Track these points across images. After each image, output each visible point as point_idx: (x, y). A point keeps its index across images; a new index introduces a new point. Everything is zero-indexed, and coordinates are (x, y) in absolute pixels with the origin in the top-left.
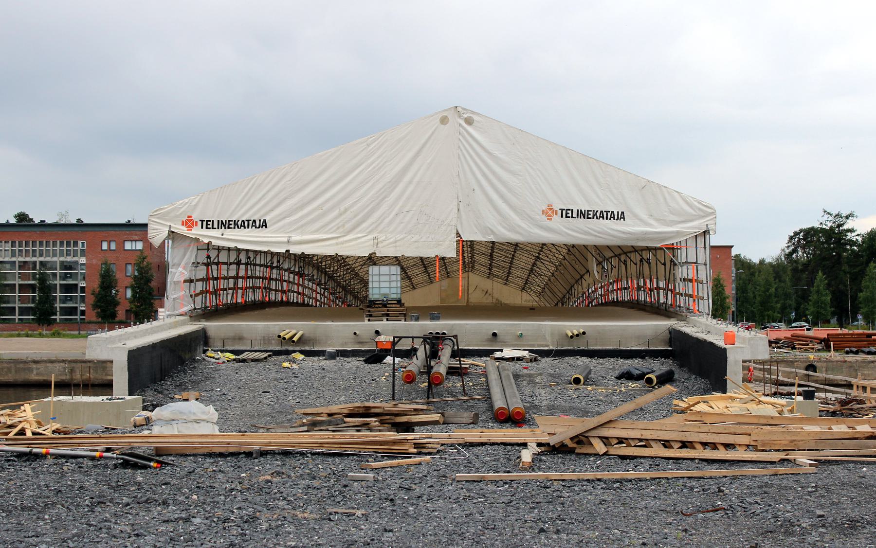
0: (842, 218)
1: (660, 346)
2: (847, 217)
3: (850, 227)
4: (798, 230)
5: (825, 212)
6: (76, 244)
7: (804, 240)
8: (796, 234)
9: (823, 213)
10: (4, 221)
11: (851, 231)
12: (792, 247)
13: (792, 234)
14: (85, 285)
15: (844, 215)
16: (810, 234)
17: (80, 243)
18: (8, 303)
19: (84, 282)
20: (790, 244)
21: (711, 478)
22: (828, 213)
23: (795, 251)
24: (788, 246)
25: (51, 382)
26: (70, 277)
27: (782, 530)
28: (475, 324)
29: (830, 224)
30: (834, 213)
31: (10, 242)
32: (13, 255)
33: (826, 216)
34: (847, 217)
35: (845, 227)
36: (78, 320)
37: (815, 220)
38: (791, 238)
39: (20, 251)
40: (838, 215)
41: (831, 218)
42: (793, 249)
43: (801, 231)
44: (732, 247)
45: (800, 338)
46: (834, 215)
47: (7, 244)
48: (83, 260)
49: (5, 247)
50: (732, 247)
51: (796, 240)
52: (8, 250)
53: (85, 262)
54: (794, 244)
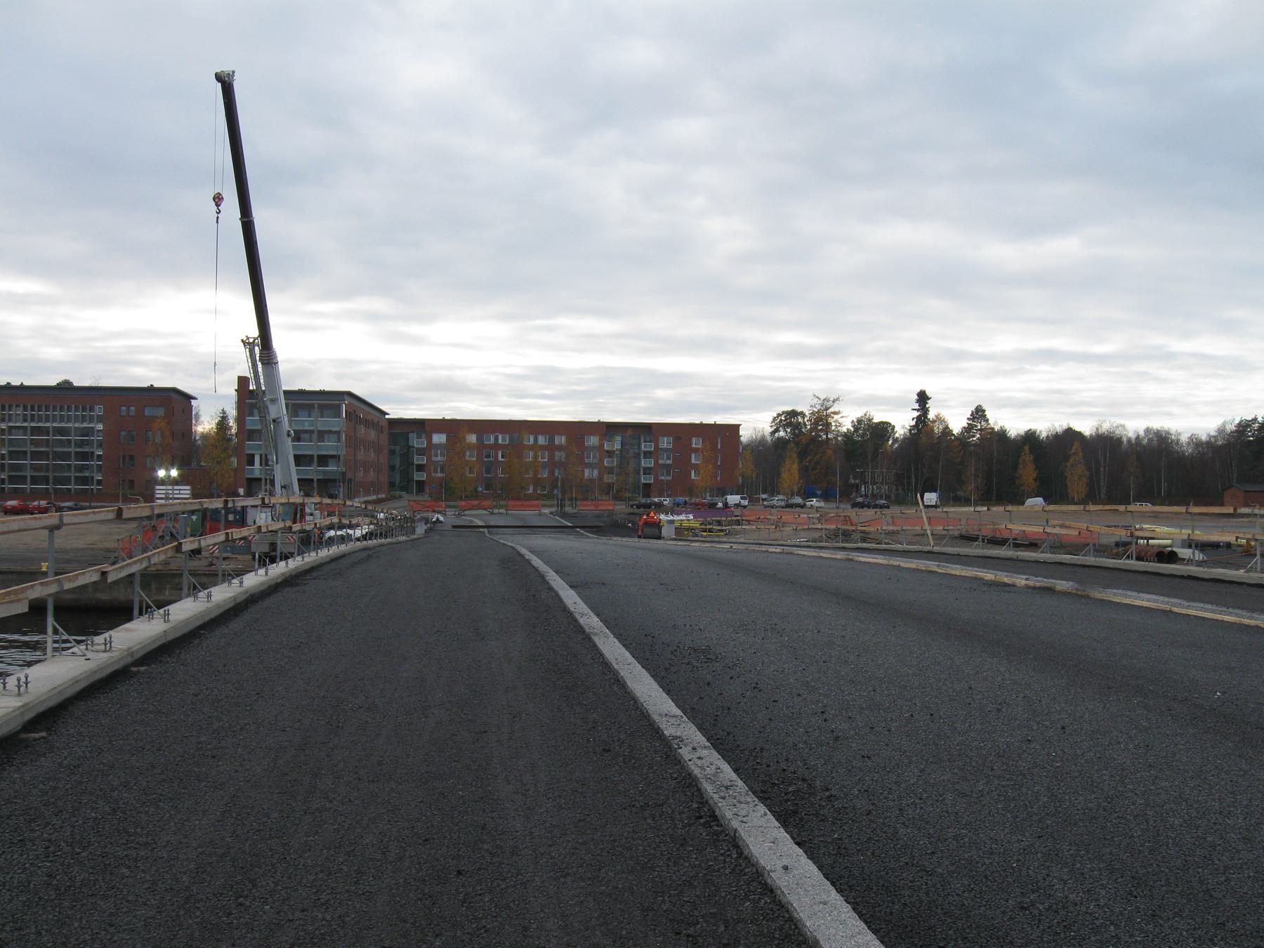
2: (834, 401)
3: (837, 410)
6: (92, 409)
9: (812, 397)
10: (3, 383)
14: (101, 453)
17: (97, 407)
18: (21, 471)
19: (100, 450)
22: (818, 398)
23: (777, 430)
24: (772, 426)
25: (327, 467)
26: (87, 445)
27: (840, 860)
31: (22, 406)
32: (25, 421)
34: (834, 401)
35: (831, 410)
36: (28, 490)
37: (919, 391)
38: (774, 419)
39: (33, 416)
40: (826, 400)
42: (775, 429)
43: (783, 413)
47: (18, 408)
48: (100, 427)
49: (16, 411)
52: (19, 415)
53: (102, 428)
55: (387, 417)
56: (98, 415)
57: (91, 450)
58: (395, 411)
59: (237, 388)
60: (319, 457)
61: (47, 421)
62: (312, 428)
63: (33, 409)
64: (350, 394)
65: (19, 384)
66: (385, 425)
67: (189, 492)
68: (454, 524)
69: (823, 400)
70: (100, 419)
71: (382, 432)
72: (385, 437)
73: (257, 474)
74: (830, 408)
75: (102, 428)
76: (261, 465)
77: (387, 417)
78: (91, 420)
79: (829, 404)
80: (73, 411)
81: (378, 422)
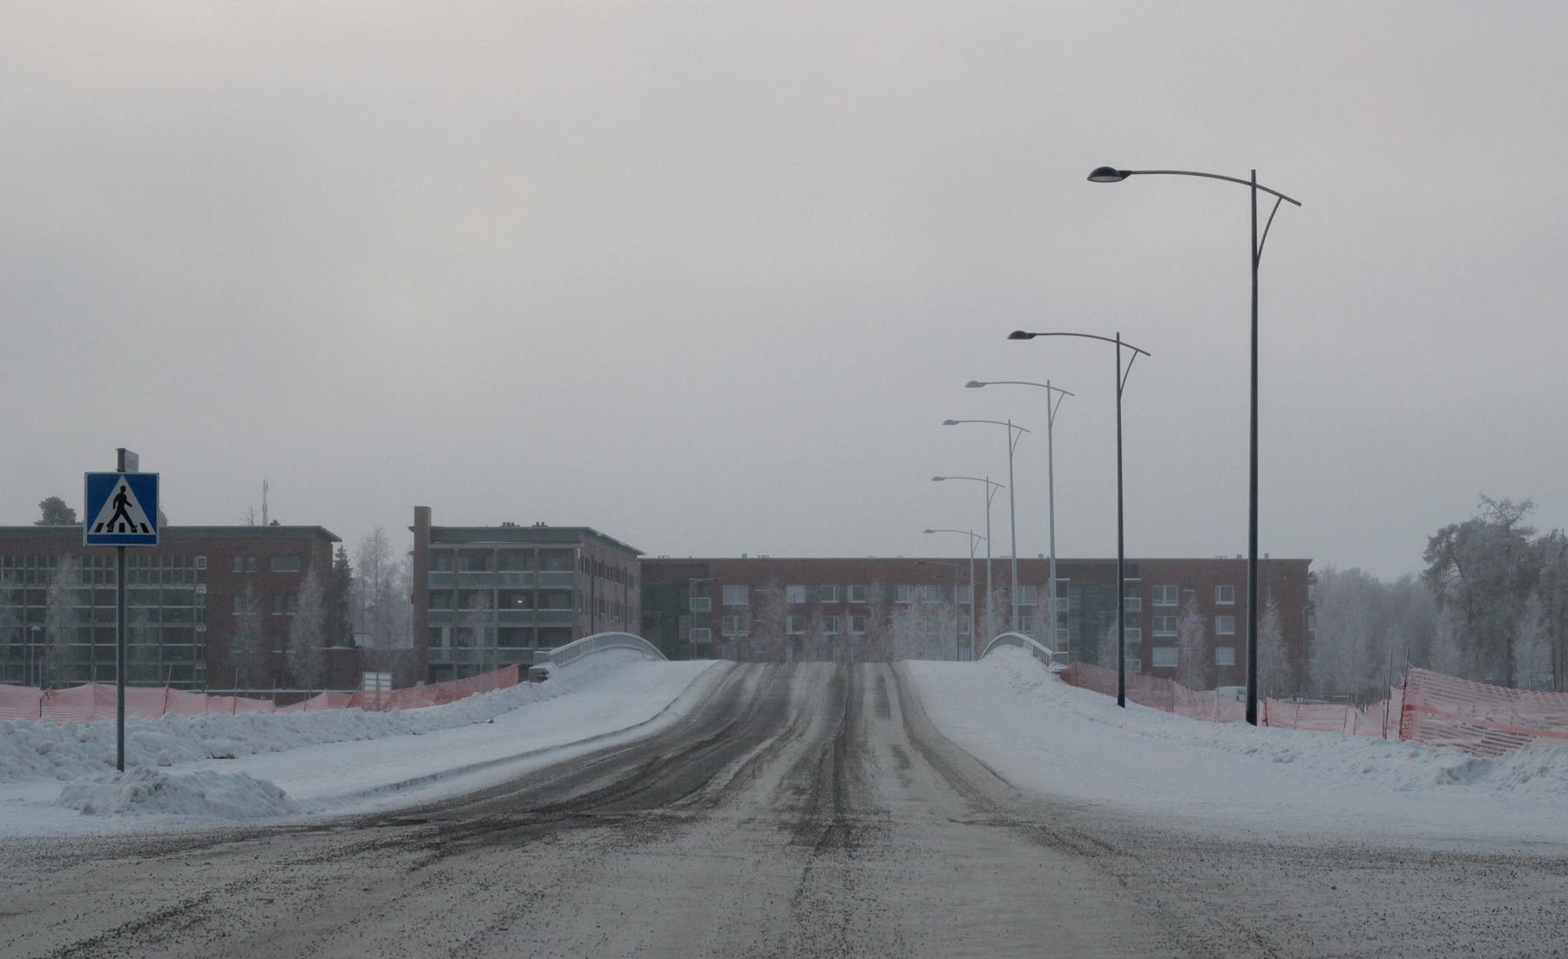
22: (1489, 501)
48: (202, 589)
55: (639, 557)
56: (199, 571)
57: (188, 625)
58: (652, 549)
59: (413, 525)
60: (541, 631)
61: (154, 580)
62: (530, 587)
63: (98, 563)
64: (589, 533)
65: (412, 535)
66: (635, 571)
67: (366, 682)
68: (1257, 172)
69: (1501, 506)
70: (202, 578)
71: (631, 585)
72: (635, 594)
73: (445, 658)
74: (1514, 521)
75: (204, 592)
76: (452, 645)
77: (639, 557)
78: (189, 580)
79: (1509, 513)
80: (25, 565)
81: (626, 569)
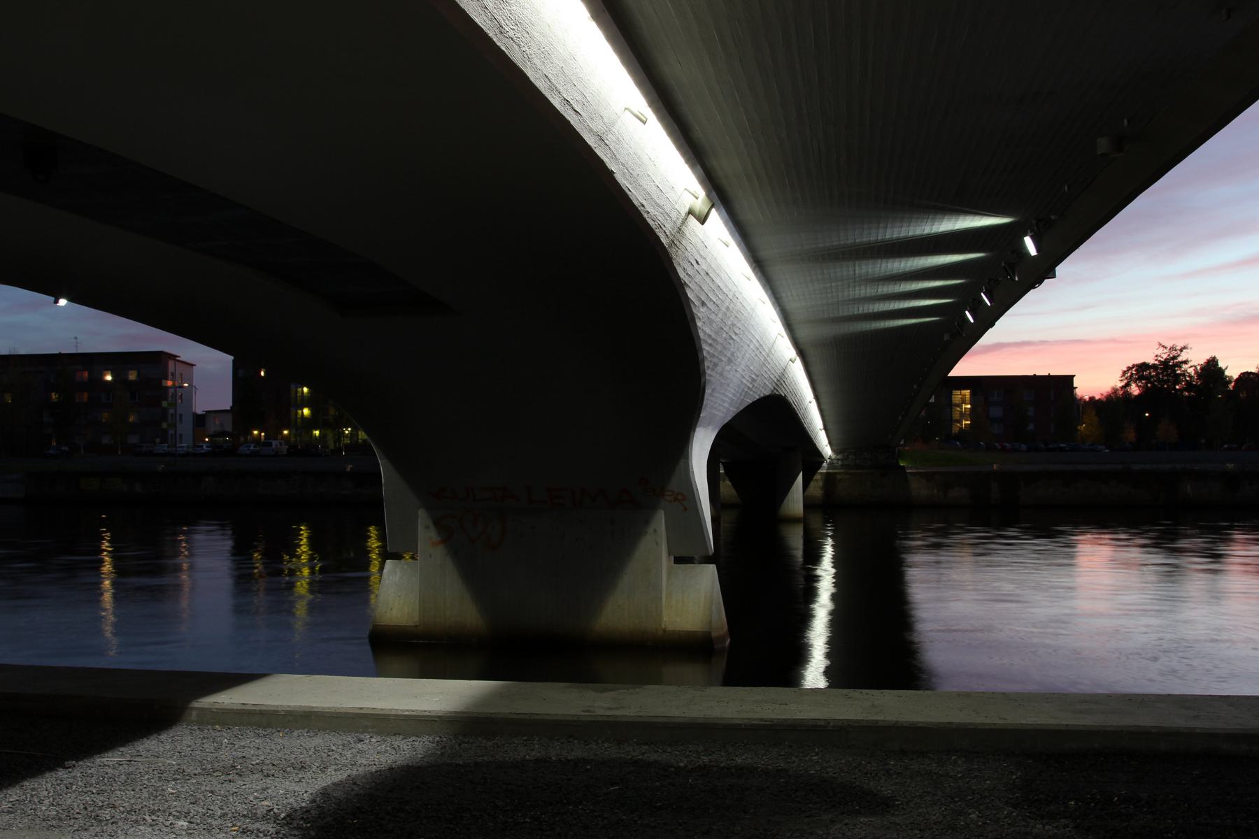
0: (1176, 350)
1: (96, 588)
4: (1130, 365)
5: (1160, 345)
7: (1136, 374)
8: (1129, 369)
11: (1186, 362)
12: (1125, 381)
13: (1126, 369)
15: (1178, 348)
16: (1141, 371)
20: (1123, 378)
21: (721, 89)
22: (1163, 346)
23: (1128, 385)
28: (839, 580)
29: (1165, 356)
30: (1169, 345)
33: (1161, 349)
35: (1180, 359)
38: (1124, 373)
40: (1173, 348)
41: (1165, 351)
43: (1134, 366)
44: (1074, 376)
45: (1181, 599)
46: (1169, 348)
50: (1074, 376)
51: (1129, 374)
54: (1126, 378)
